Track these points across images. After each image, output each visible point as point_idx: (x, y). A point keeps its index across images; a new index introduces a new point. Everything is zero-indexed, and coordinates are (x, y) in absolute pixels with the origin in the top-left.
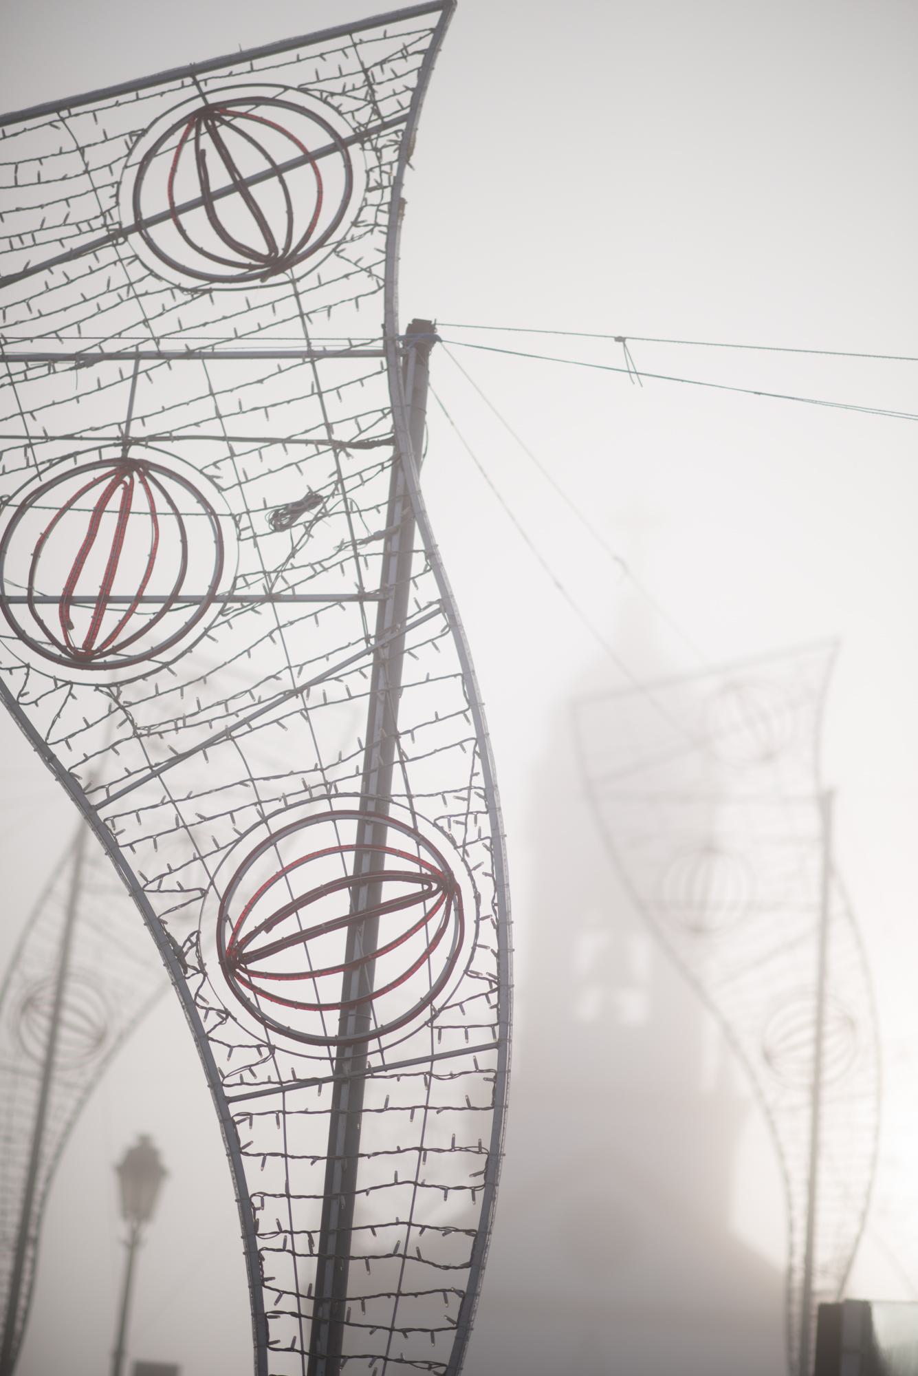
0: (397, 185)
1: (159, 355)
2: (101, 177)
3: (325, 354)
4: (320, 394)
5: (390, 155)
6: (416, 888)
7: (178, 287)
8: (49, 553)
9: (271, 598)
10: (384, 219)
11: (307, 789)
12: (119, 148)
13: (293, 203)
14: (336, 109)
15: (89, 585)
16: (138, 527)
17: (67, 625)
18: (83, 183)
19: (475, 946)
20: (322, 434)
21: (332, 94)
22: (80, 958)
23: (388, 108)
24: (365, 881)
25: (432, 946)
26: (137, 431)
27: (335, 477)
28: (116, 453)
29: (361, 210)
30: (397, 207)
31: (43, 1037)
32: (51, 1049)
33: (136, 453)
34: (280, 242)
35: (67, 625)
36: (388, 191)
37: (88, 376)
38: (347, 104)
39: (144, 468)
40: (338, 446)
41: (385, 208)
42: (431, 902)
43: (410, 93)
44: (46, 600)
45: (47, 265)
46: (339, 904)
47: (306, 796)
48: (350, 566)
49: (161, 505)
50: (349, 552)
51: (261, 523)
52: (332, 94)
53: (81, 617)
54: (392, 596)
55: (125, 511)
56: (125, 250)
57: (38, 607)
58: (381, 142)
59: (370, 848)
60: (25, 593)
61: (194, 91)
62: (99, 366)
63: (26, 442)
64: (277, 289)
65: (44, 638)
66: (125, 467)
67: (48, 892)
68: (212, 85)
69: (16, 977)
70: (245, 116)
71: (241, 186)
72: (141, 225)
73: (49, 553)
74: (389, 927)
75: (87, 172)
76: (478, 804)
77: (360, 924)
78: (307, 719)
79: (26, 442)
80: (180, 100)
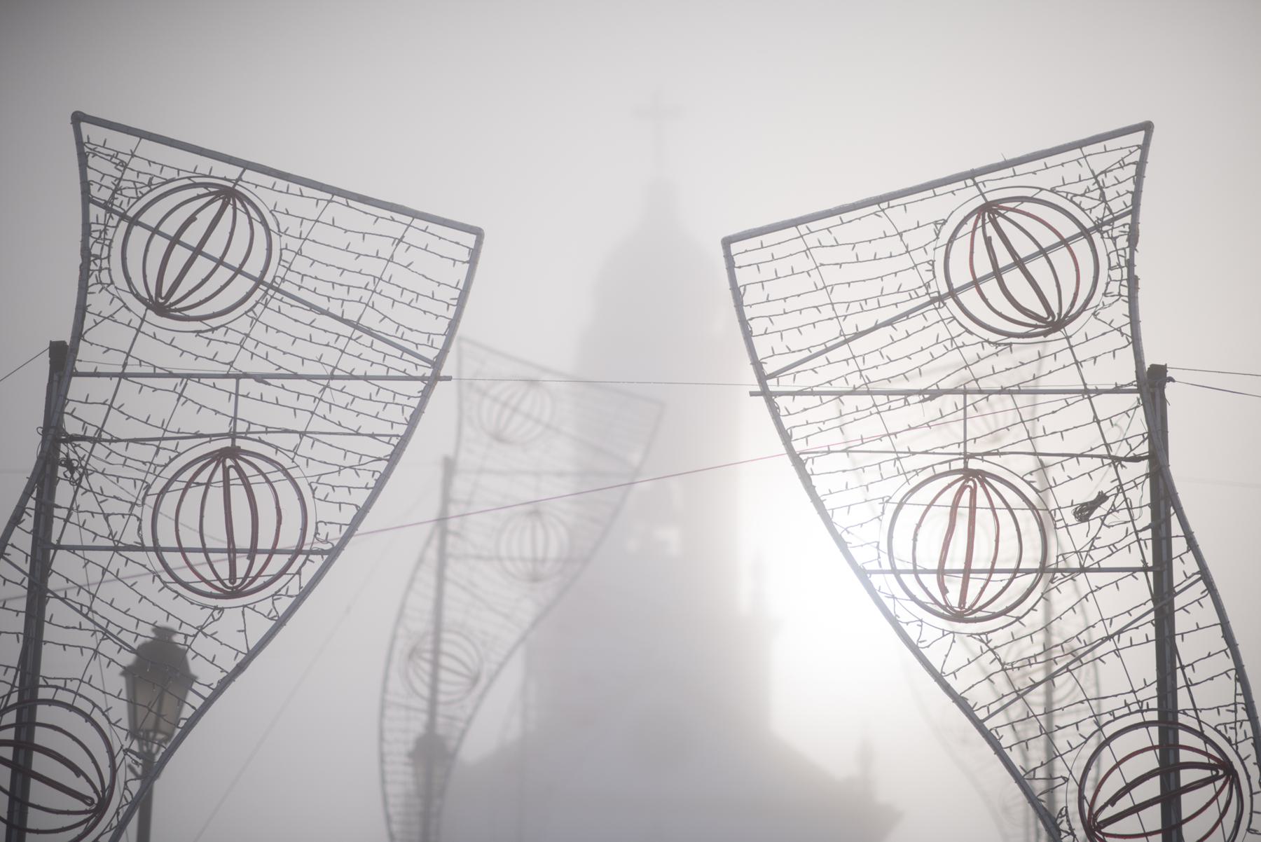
0: (1130, 264)
1: (980, 392)
2: (919, 256)
3: (1099, 392)
4: (1099, 422)
5: (1122, 242)
6: (1206, 774)
7: (987, 341)
9: (1083, 570)
10: (1125, 291)
11: (1127, 705)
12: (929, 233)
13: (1062, 276)
14: (1079, 206)
15: (956, 560)
16: (984, 516)
17: (944, 591)
18: (906, 262)
19: (1252, 812)
20: (1103, 451)
21: (1075, 195)
22: (451, 614)
23: (1117, 206)
24: (1169, 768)
25: (1223, 815)
26: (971, 448)
27: (1117, 483)
28: (959, 465)
29: (1108, 284)
30: (1133, 282)
31: (427, 679)
32: (434, 689)
33: (974, 464)
34: (1055, 310)
35: (944, 591)
36: (1125, 270)
37: (933, 407)
38: (1086, 203)
39: (981, 476)
40: (1116, 461)
41: (1125, 283)
42: (1219, 783)
43: (1130, 196)
44: (926, 571)
45: (890, 323)
46: (1152, 788)
47: (1126, 711)
48: (1135, 546)
50: (1133, 537)
51: (1071, 519)
52: (1075, 195)
54: (1161, 568)
55: (973, 508)
56: (944, 313)
57: (921, 576)
58: (1116, 233)
59: (1168, 747)
60: (911, 567)
61: (974, 190)
62: (938, 400)
63: (894, 456)
64: (1056, 341)
65: (930, 600)
66: (968, 474)
67: (421, 561)
68: (990, 186)
69: (401, 631)
70: (1013, 210)
71: (1019, 263)
72: (953, 293)
74: (1189, 803)
75: (908, 252)
76: (1242, 715)
77: (1170, 799)
78: (1119, 656)
79: (894, 456)
80: (967, 199)
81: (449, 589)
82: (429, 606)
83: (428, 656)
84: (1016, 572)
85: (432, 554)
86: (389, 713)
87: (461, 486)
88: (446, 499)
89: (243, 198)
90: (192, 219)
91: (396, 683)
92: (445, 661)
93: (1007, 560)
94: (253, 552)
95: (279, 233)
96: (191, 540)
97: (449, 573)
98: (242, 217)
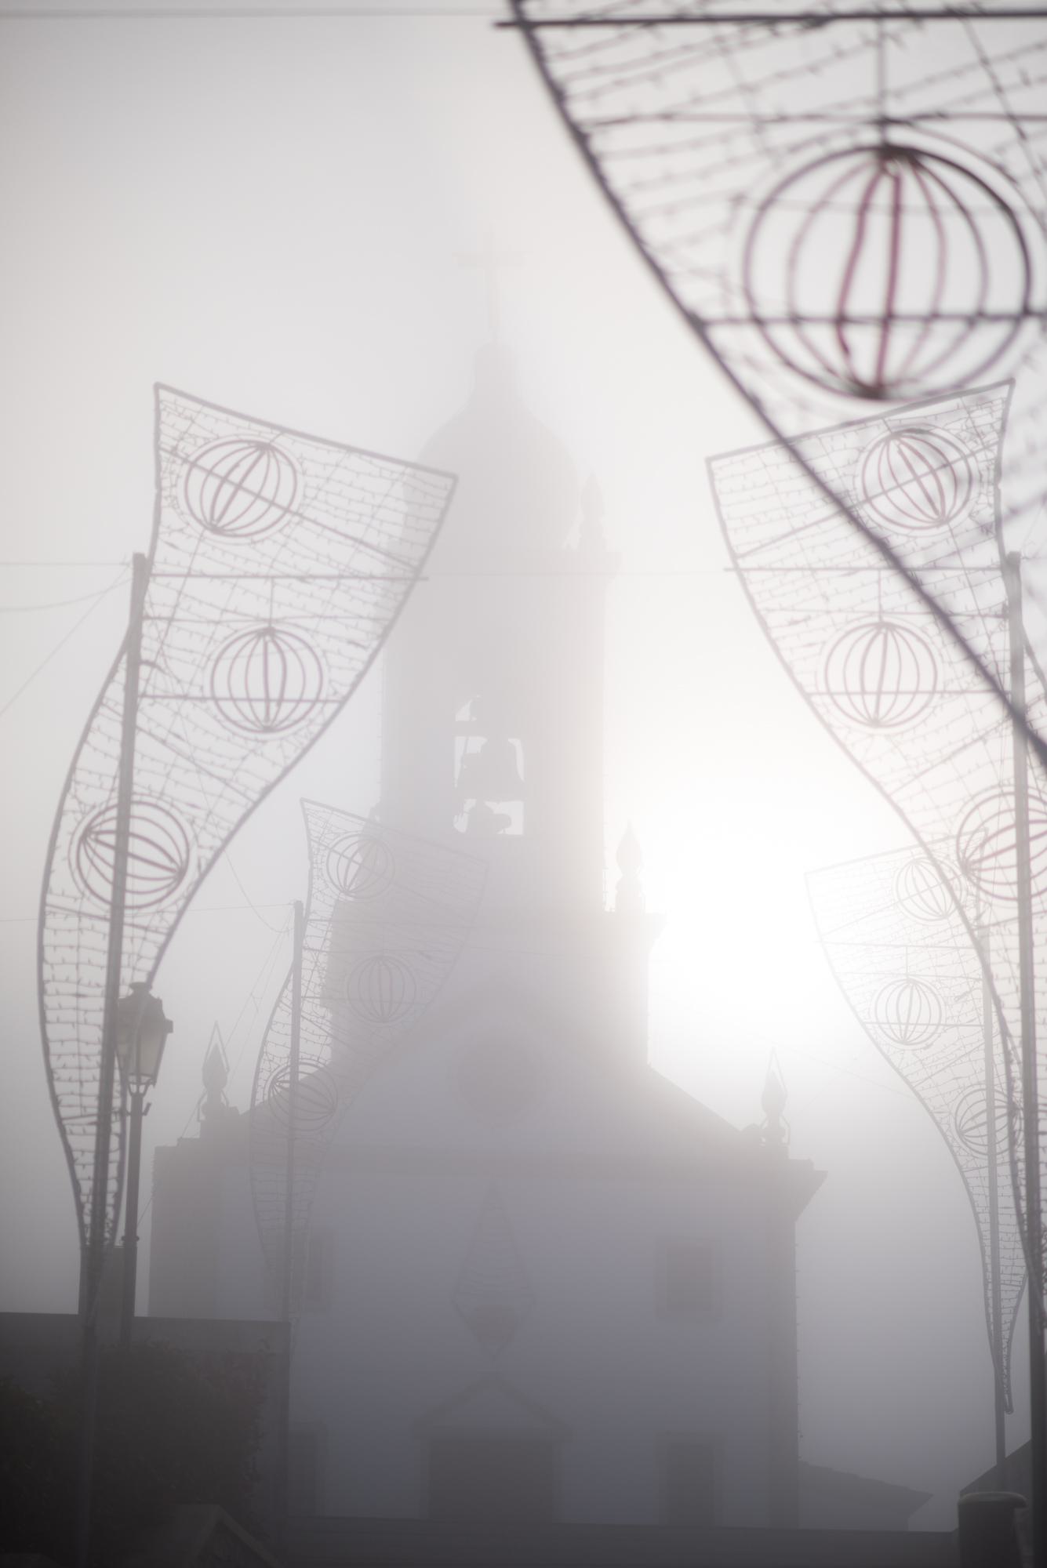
8: (957, 259)
15: (867, 299)
26: (894, 109)
31: (109, 873)
44: (860, 321)
49: (941, 199)
53: (863, 340)
55: (897, 210)
66: (888, 153)
69: (70, 804)
73: (957, 259)
81: (141, 741)
82: (112, 767)
83: (111, 839)
84: (915, 693)
85: (116, 693)
86: (50, 921)
87: (159, 594)
88: (138, 615)
89: (274, 449)
90: (236, 465)
91: (62, 877)
92: (135, 846)
93: (908, 684)
94: (281, 700)
95: (304, 473)
96: (239, 692)
97: (141, 720)
98: (273, 461)
